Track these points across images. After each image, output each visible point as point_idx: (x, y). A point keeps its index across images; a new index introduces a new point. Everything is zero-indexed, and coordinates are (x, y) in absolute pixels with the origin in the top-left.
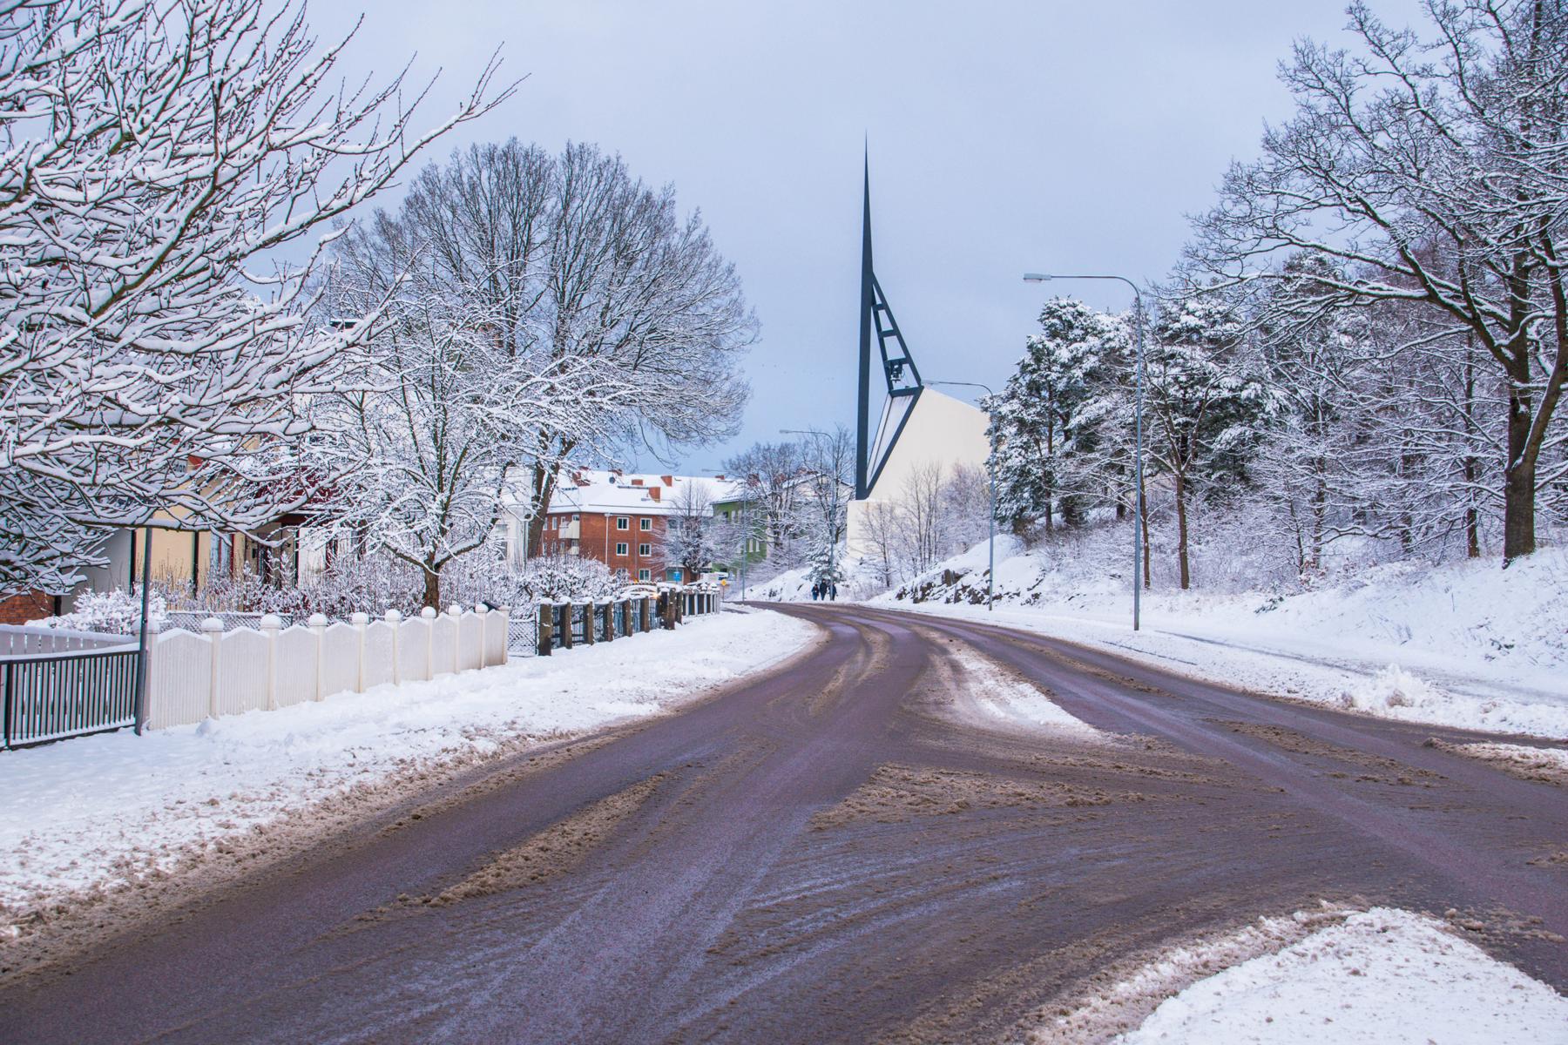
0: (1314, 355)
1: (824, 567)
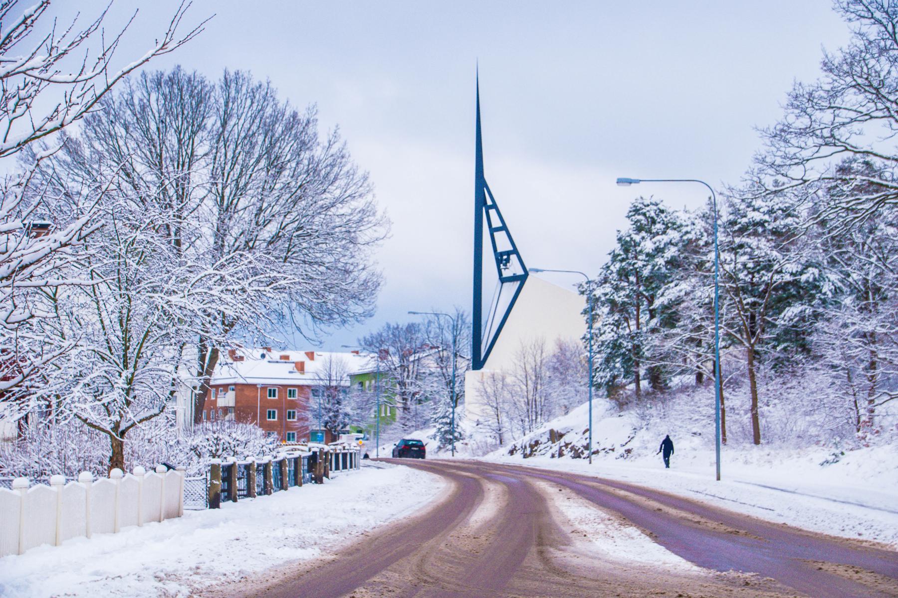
0: (863, 244)
1: (446, 428)
